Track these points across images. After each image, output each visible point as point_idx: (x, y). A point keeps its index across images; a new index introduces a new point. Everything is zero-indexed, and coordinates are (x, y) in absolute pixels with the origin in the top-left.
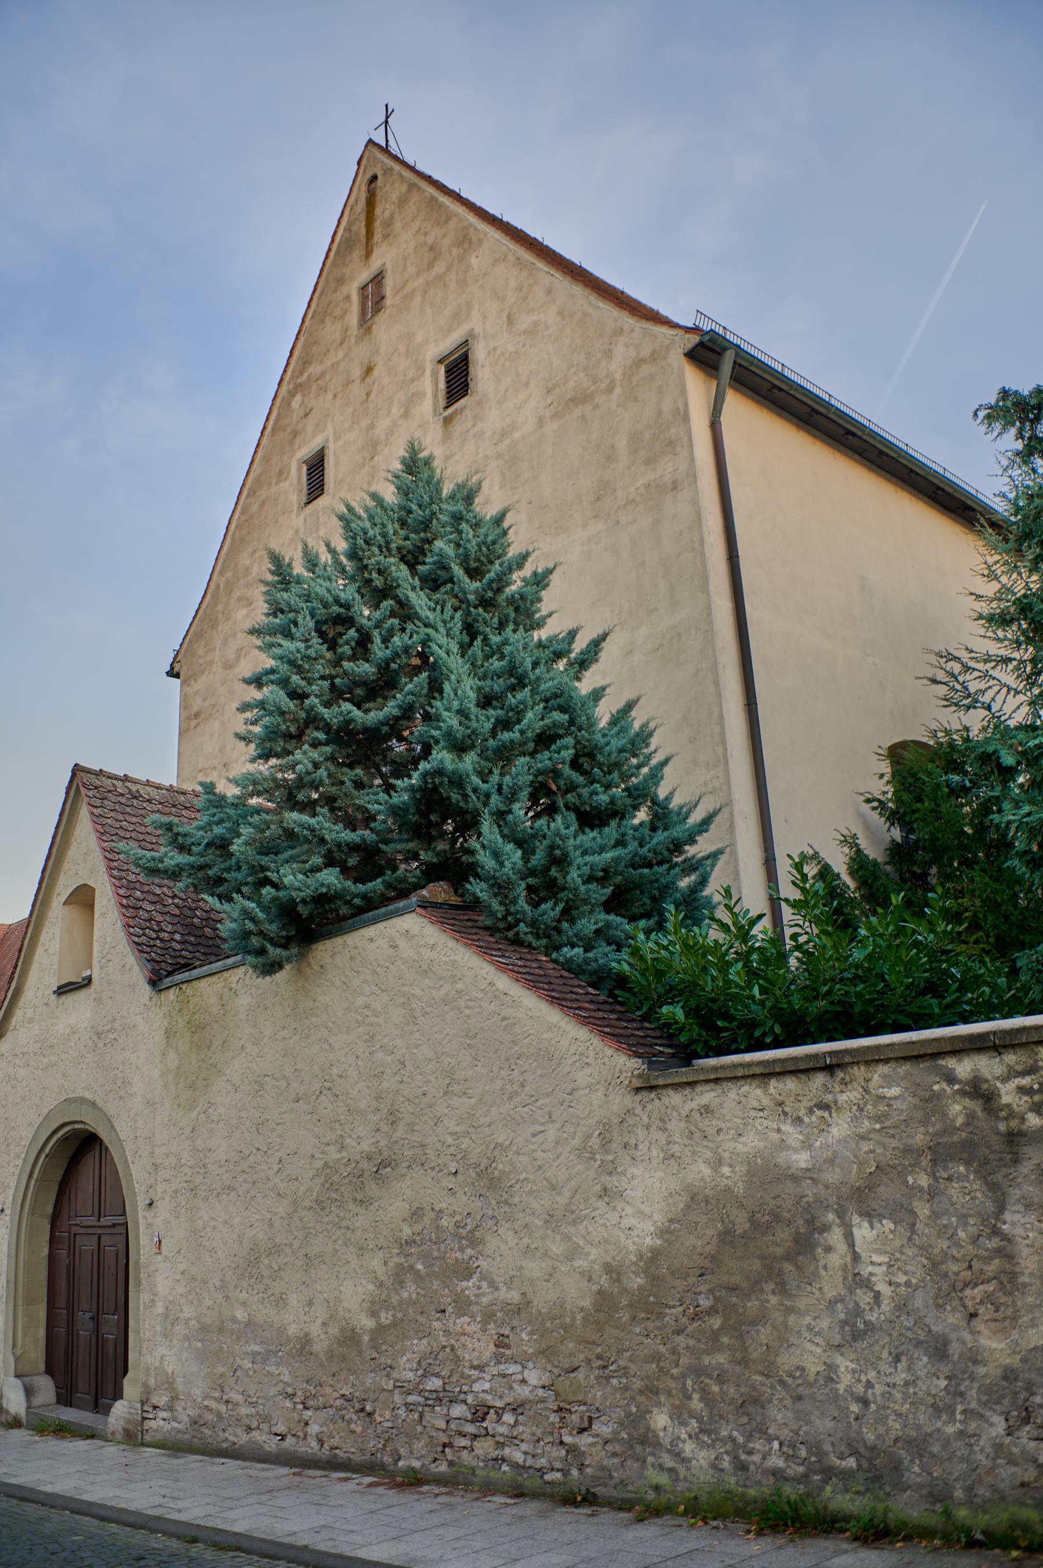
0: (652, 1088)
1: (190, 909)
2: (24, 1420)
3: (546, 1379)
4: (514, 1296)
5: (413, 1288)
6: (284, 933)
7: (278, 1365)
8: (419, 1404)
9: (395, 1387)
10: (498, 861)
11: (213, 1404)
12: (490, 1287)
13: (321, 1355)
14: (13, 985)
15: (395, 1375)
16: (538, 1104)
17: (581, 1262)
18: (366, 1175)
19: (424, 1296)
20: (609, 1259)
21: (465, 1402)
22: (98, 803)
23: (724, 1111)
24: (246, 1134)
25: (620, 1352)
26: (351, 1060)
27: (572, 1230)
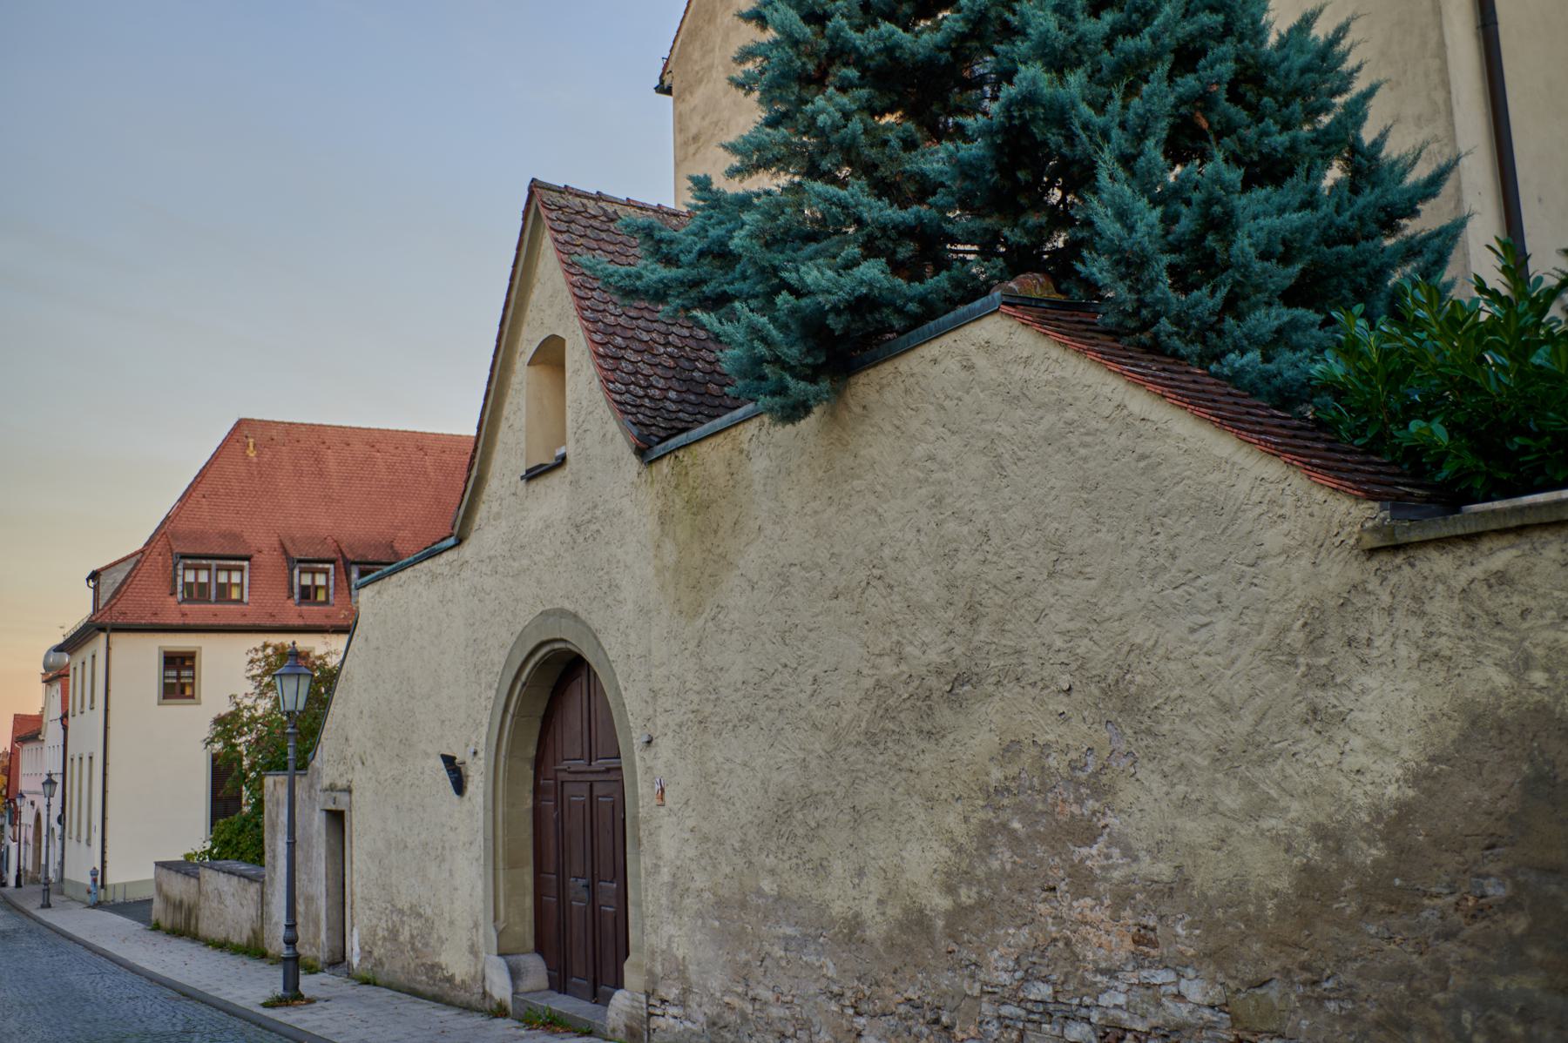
0: (1396, 548)
1: (688, 359)
2: (510, 1008)
3: (1216, 994)
4: (1163, 870)
5: (1007, 854)
6: (809, 360)
7: (818, 954)
8: (1018, 1018)
9: (982, 992)
10: (1124, 225)
11: (736, 1002)
12: (1124, 856)
13: (878, 944)
14: (474, 473)
15: (982, 976)
16: (1199, 582)
17: (1274, 822)
18: (935, 697)
19: (1024, 867)
20: (1321, 818)
21: (1088, 1020)
22: (564, 227)
23: (1536, 580)
24: (769, 646)
25: (1341, 961)
26: (910, 535)
27: (1258, 773)
